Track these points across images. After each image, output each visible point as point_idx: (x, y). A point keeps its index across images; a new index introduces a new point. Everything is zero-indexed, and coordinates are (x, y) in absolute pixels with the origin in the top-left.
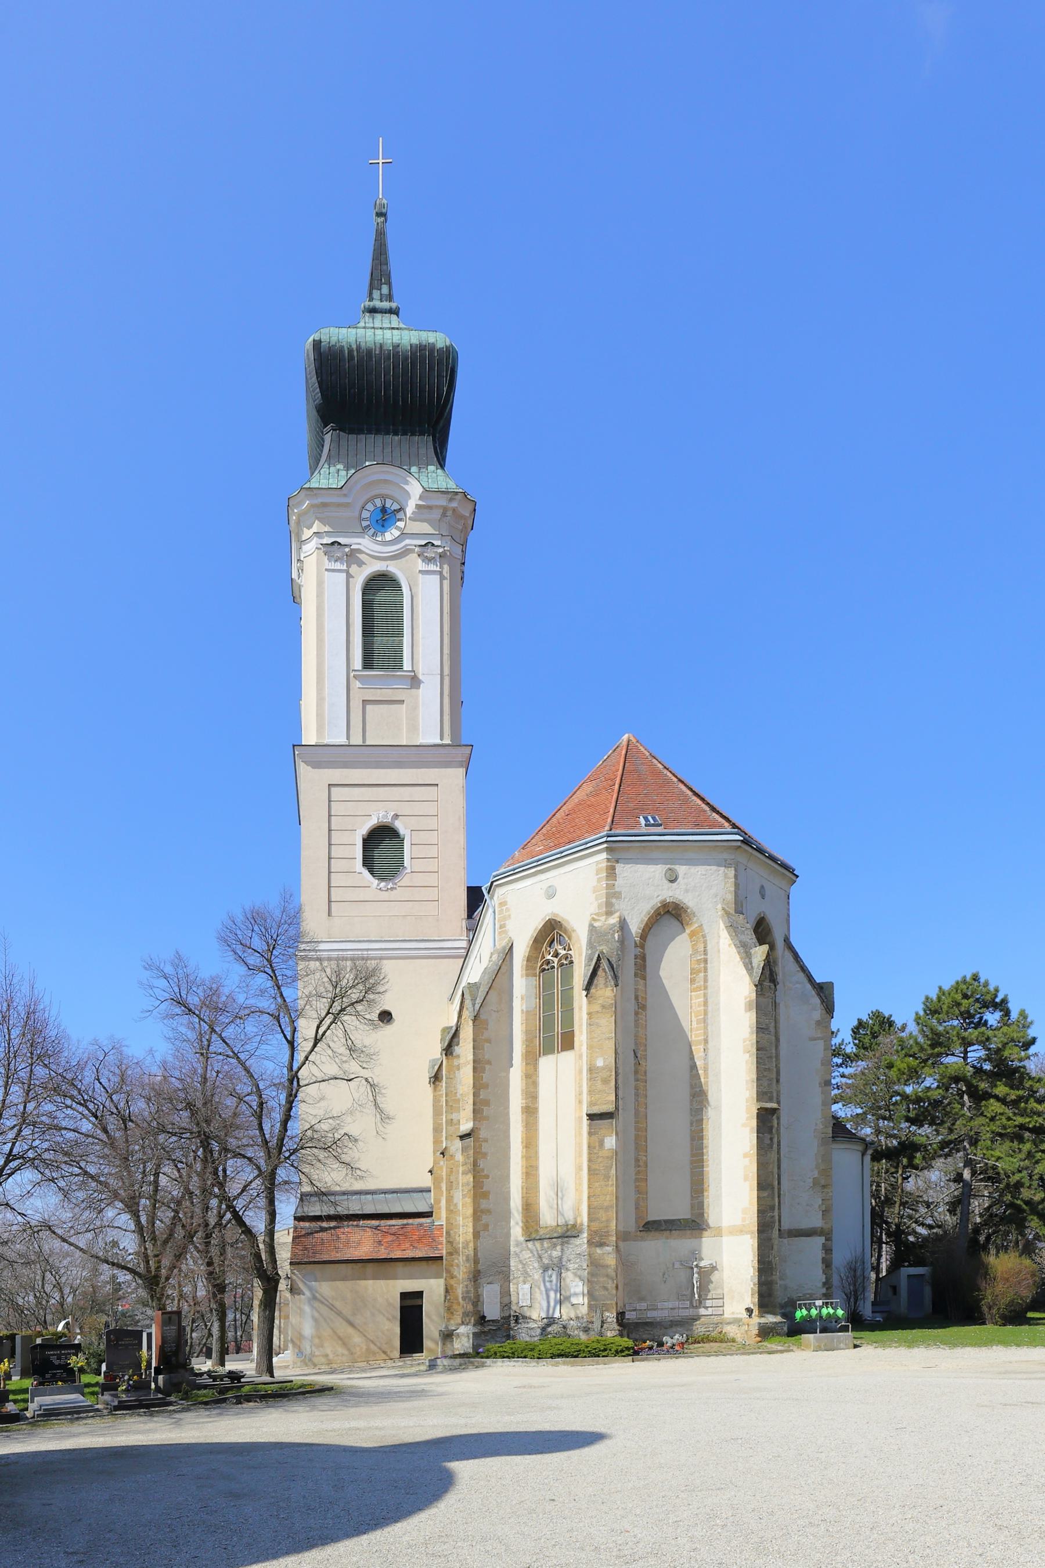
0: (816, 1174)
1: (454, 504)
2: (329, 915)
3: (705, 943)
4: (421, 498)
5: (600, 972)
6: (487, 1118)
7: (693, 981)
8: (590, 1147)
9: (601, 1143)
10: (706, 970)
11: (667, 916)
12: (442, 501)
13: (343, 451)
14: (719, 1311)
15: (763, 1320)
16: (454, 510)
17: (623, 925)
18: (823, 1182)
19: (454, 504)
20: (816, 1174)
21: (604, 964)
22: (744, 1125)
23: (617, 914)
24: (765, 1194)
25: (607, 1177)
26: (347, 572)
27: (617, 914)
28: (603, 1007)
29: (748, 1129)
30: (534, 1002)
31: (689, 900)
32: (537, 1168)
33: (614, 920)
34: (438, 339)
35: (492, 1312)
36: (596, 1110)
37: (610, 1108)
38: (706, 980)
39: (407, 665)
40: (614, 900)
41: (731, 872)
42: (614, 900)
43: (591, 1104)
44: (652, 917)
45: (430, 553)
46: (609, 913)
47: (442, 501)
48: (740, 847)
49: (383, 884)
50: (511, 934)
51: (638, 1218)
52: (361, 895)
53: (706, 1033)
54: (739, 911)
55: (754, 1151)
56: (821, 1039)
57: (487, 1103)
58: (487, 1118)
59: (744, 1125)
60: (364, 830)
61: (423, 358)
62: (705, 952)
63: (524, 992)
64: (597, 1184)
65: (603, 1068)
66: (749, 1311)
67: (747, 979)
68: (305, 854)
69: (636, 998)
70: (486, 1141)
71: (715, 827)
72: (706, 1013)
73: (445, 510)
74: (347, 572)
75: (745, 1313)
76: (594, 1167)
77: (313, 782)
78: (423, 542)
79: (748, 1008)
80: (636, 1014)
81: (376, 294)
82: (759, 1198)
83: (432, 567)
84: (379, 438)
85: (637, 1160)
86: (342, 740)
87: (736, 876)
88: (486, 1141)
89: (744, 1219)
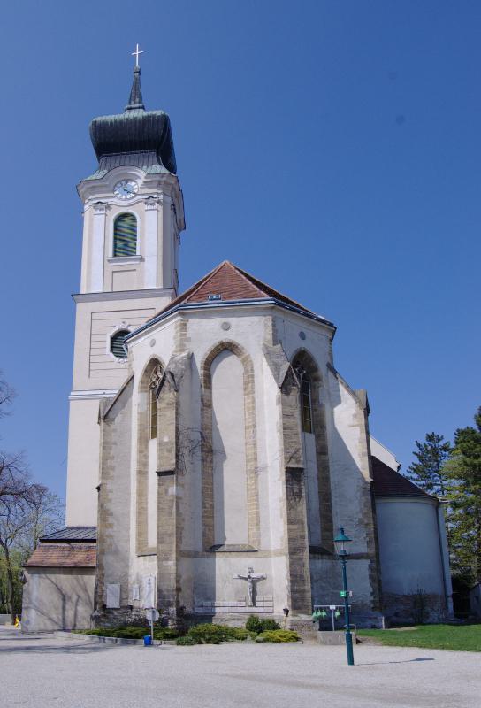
0: (360, 516)
1: (165, 179)
2: (89, 376)
3: (252, 364)
4: (146, 178)
5: (166, 383)
6: (112, 478)
7: (245, 389)
8: (159, 493)
9: (167, 491)
10: (253, 382)
11: (227, 351)
12: (158, 178)
13: (108, 164)
14: (270, 610)
15: (296, 619)
16: (165, 181)
17: (191, 357)
18: (366, 522)
19: (165, 179)
20: (360, 516)
21: (168, 376)
22: (279, 480)
23: (187, 351)
24: (295, 527)
25: (170, 514)
26: (106, 215)
27: (187, 351)
28: (168, 404)
29: (281, 482)
30: (145, 407)
31: (239, 340)
32: (146, 509)
33: (184, 354)
34: (159, 113)
35: (112, 602)
36: (162, 470)
37: (172, 468)
38: (253, 388)
39: (138, 253)
40: (185, 343)
41: (269, 320)
42: (185, 343)
43: (160, 466)
44: (213, 351)
45: (151, 201)
46: (182, 350)
47: (158, 178)
48: (273, 308)
49: (121, 360)
50: (134, 369)
51: (204, 543)
52: (109, 366)
53: (254, 420)
54: (276, 341)
55: (285, 497)
56: (358, 425)
57: (113, 468)
58: (112, 478)
59: (279, 480)
60: (112, 332)
61: (149, 121)
62: (252, 370)
63: (139, 401)
64: (163, 518)
65: (167, 443)
66: (286, 611)
67: (276, 385)
68: (77, 346)
69: (202, 400)
70: (111, 491)
71: (254, 296)
72: (254, 408)
73: (159, 182)
74: (106, 215)
75: (283, 611)
76: (161, 506)
77: (83, 310)
78: (147, 197)
79: (278, 404)
80: (202, 410)
81: (133, 102)
82: (290, 530)
83: (152, 207)
84: (132, 156)
85: (204, 504)
86: (101, 291)
87: (274, 325)
88: (111, 491)
89: (282, 545)
